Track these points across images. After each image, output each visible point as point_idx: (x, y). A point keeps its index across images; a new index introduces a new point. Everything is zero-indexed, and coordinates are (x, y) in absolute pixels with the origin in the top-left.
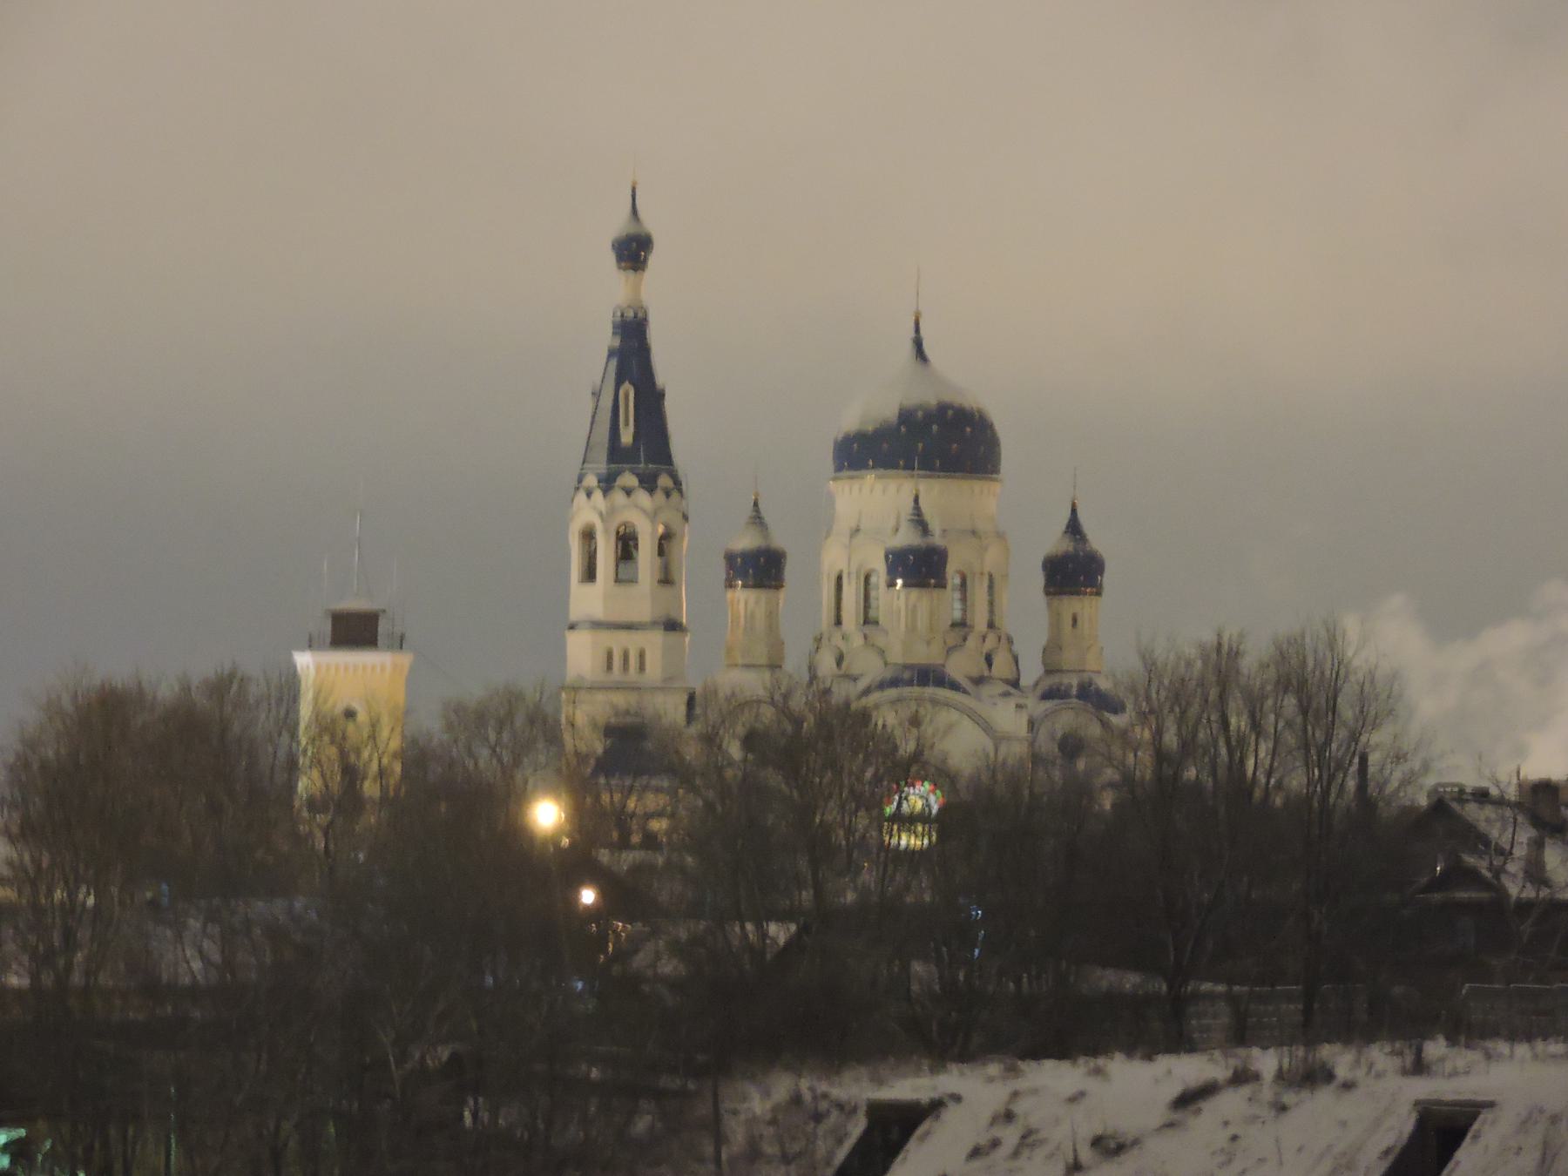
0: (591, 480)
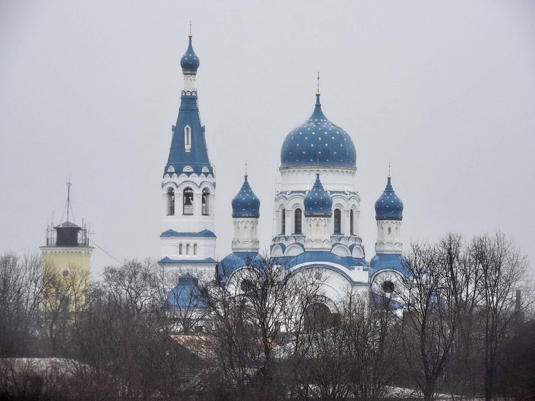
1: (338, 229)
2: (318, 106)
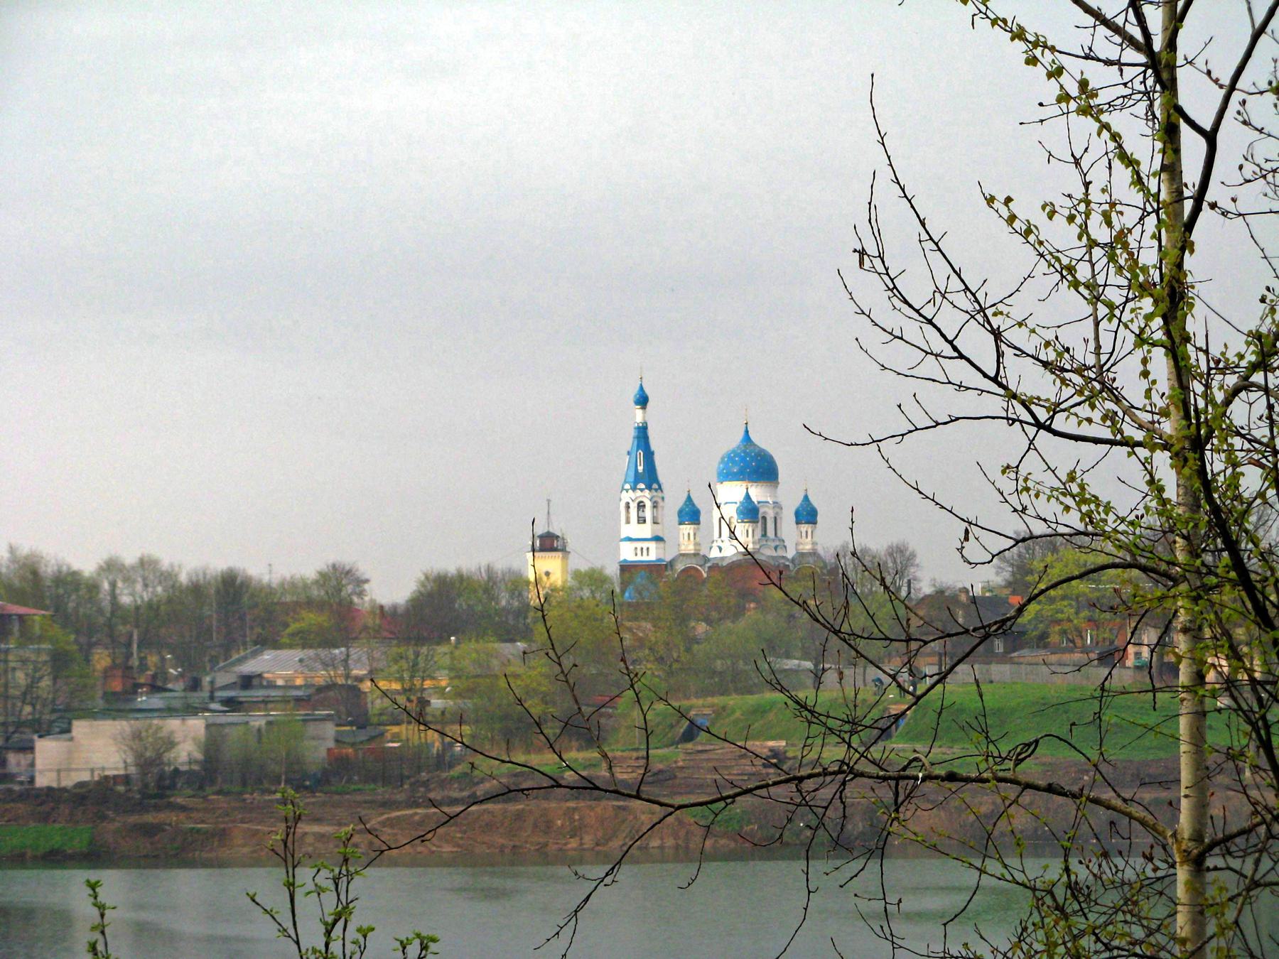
0: (627, 486)
1: (765, 534)
2: (747, 432)
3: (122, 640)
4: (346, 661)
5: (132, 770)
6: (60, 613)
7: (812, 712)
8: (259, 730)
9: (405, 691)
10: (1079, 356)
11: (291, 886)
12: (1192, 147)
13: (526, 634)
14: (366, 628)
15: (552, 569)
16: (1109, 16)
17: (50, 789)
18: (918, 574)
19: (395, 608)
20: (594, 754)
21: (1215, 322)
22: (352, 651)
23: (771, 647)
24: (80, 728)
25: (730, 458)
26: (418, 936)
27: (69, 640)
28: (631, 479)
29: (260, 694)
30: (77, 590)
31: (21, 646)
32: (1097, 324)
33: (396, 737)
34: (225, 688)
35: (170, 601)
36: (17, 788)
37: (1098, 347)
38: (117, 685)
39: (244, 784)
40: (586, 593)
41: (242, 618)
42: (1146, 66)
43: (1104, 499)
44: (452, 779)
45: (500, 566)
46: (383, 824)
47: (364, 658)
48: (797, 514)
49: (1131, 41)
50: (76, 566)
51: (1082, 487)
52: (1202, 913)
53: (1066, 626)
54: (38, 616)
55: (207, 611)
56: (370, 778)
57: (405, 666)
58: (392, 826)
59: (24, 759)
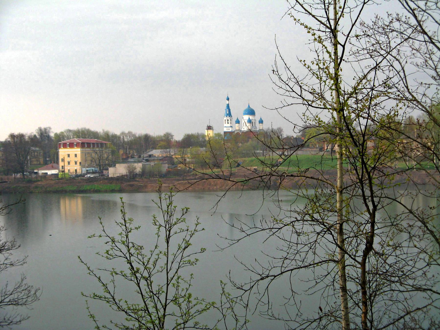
1: (253, 126)
3: (126, 148)
4: (170, 152)
5: (128, 174)
6: (114, 143)
7: (264, 163)
8: (153, 166)
9: (181, 158)
10: (317, 91)
11: (160, 198)
12: (340, 48)
13: (205, 146)
14: (173, 145)
15: (211, 133)
16: (323, 22)
17: (112, 177)
18: (283, 133)
19: (179, 141)
20: (219, 170)
21: (345, 84)
22: (171, 150)
23: (255, 148)
24: (117, 165)
25: (246, 110)
26: (186, 208)
27: (115, 148)
28: (226, 115)
29: (153, 158)
30: (116, 138)
31: (105, 149)
32: (321, 84)
33: (180, 167)
34: (145, 157)
35: (134, 140)
36: (105, 177)
37: (321, 89)
38: (124, 157)
39: (150, 176)
40: (217, 138)
41: (149, 143)
42: (330, 32)
43: (324, 121)
44: (191, 175)
45: (200, 132)
46: (177, 184)
47: (173, 151)
48: (259, 121)
49: (327, 27)
50: (116, 133)
51: (319, 119)
52: (342, 202)
53: (313, 143)
54: (109, 143)
55: (142, 142)
56: (175, 175)
57: (181, 152)
58: (179, 184)
59: (107, 172)
